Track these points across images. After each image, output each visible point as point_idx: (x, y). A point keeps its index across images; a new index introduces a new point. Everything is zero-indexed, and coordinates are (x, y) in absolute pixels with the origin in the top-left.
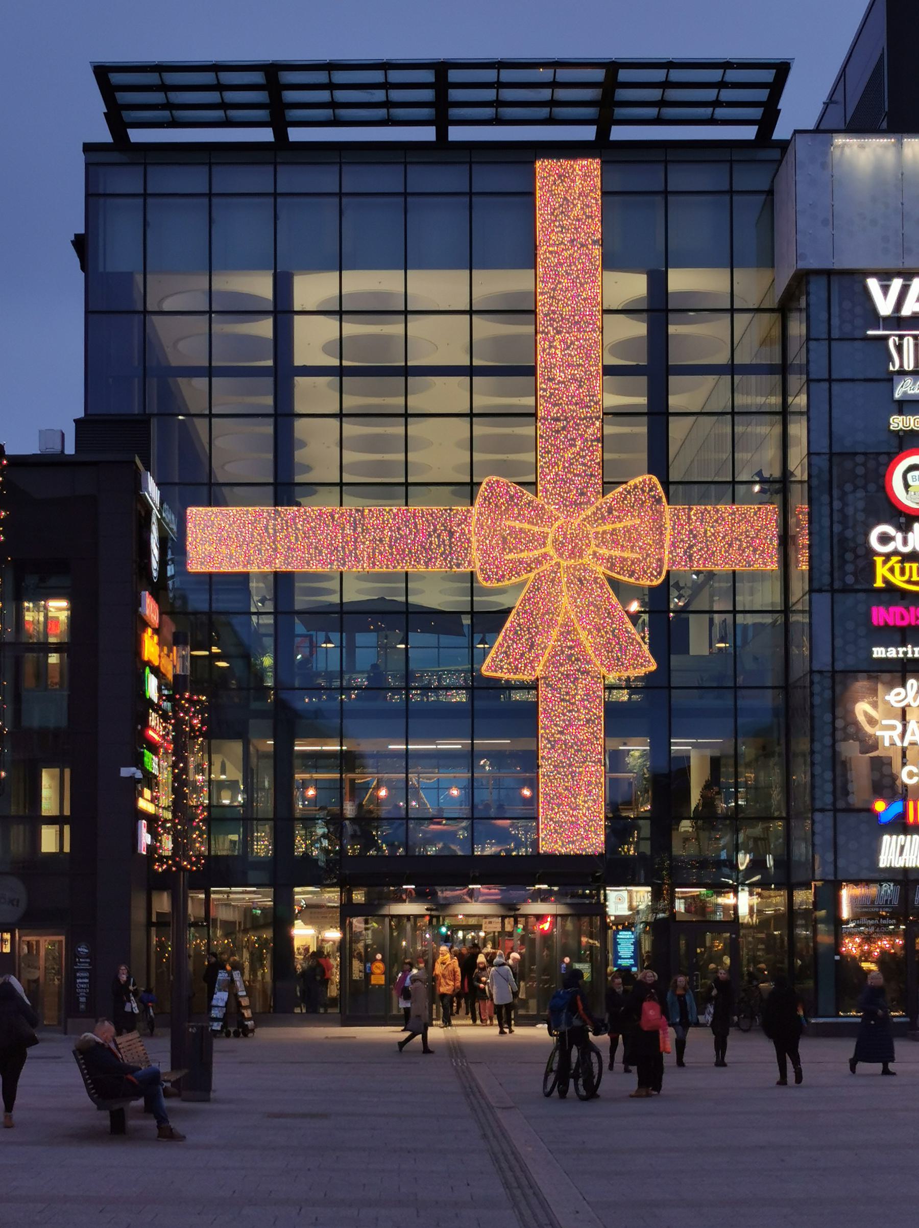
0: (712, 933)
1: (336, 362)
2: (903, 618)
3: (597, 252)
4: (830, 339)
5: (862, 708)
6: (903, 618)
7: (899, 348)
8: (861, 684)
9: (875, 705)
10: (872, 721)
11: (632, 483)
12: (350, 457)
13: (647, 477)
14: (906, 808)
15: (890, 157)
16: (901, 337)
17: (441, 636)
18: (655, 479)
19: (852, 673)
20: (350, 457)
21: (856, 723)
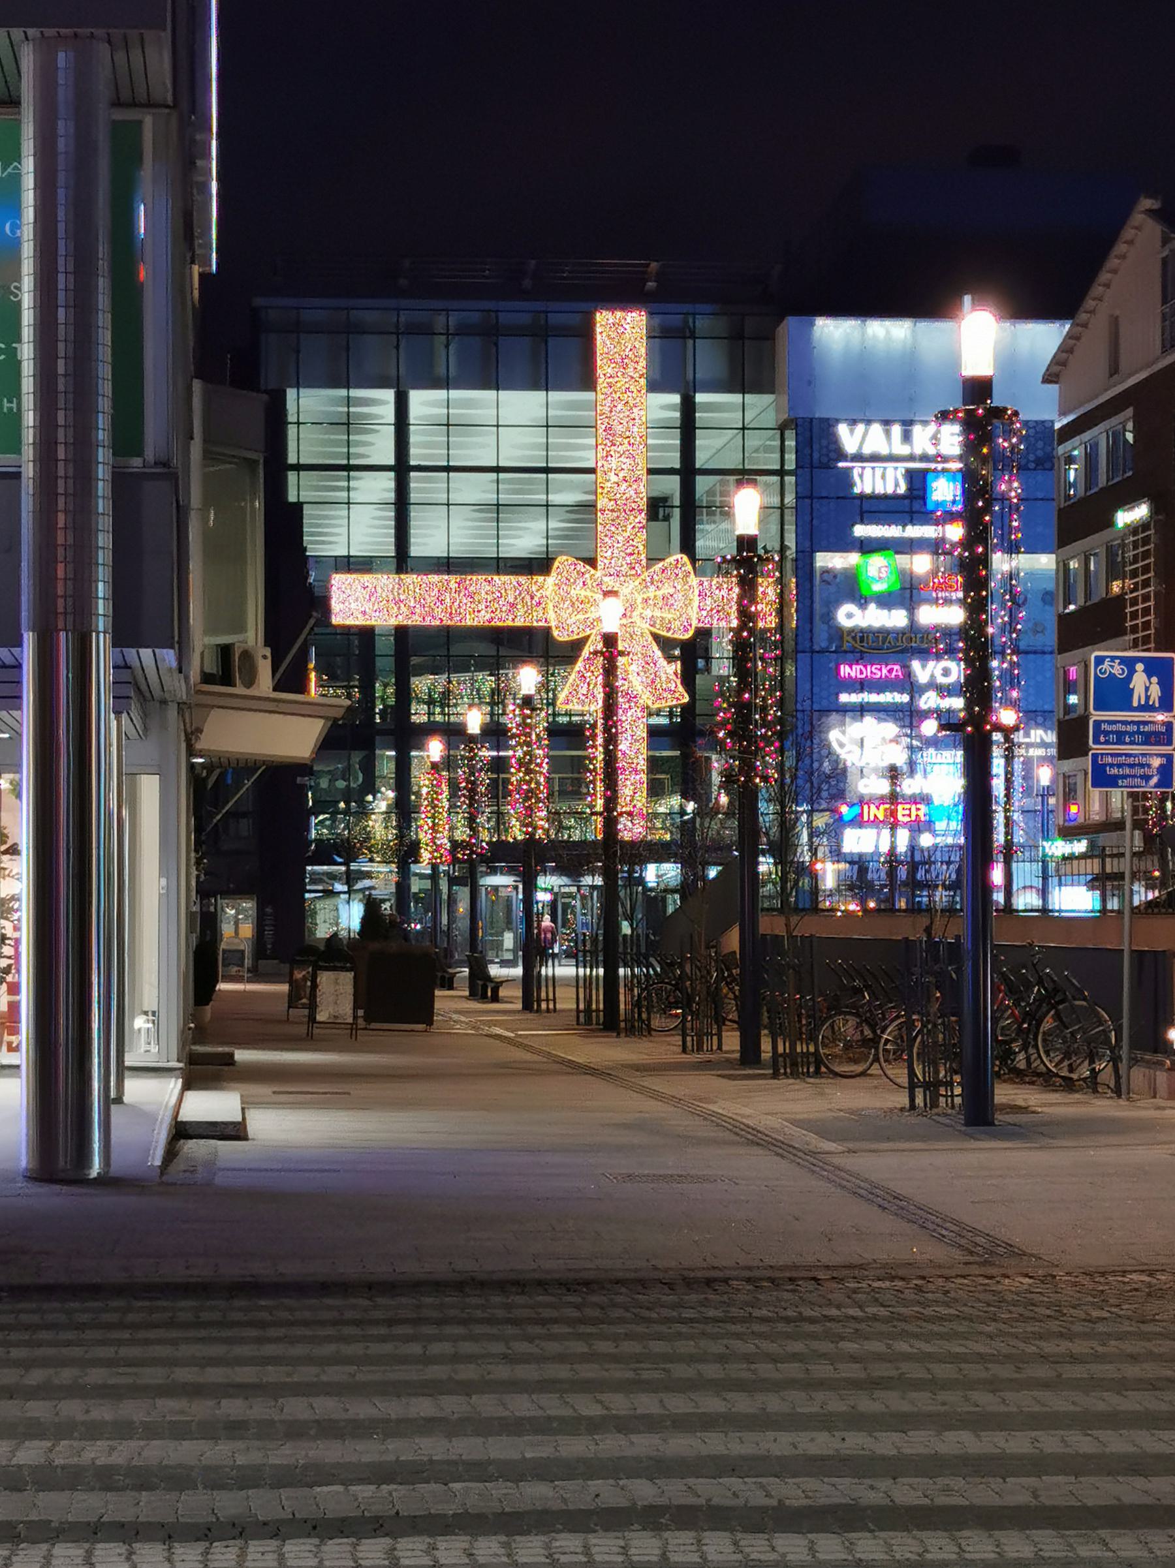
0: (217, 982)
1: (550, 476)
2: (861, 673)
3: (643, 382)
4: (812, 467)
5: (834, 736)
6: (861, 673)
7: (861, 476)
8: (834, 717)
9: (844, 733)
10: (842, 745)
11: (668, 560)
12: (550, 541)
13: (679, 556)
14: (862, 809)
15: (856, 335)
16: (863, 468)
17: (393, 659)
18: (685, 558)
19: (827, 711)
20: (550, 541)
21: (829, 746)
